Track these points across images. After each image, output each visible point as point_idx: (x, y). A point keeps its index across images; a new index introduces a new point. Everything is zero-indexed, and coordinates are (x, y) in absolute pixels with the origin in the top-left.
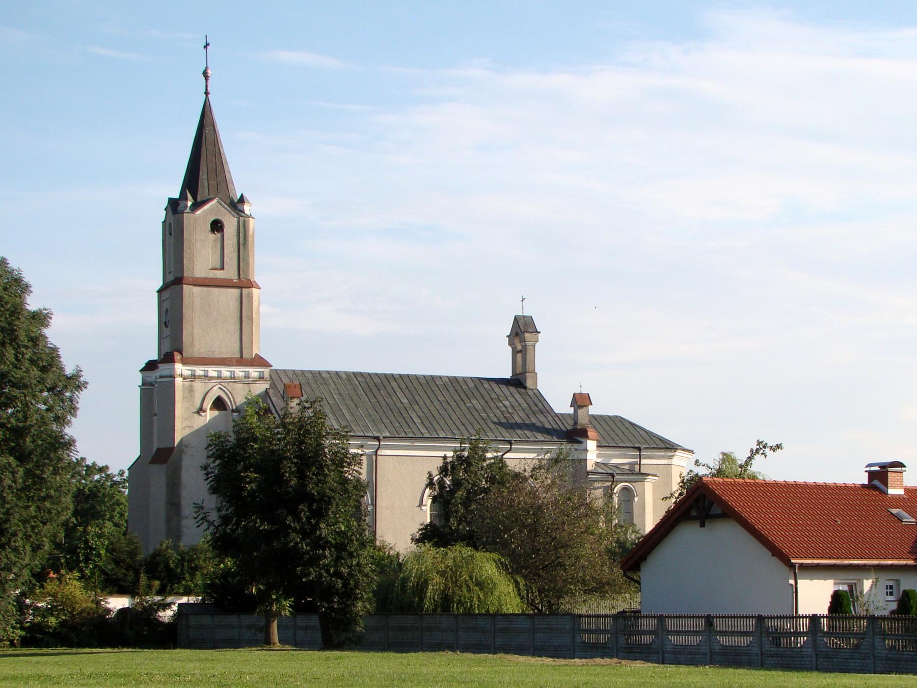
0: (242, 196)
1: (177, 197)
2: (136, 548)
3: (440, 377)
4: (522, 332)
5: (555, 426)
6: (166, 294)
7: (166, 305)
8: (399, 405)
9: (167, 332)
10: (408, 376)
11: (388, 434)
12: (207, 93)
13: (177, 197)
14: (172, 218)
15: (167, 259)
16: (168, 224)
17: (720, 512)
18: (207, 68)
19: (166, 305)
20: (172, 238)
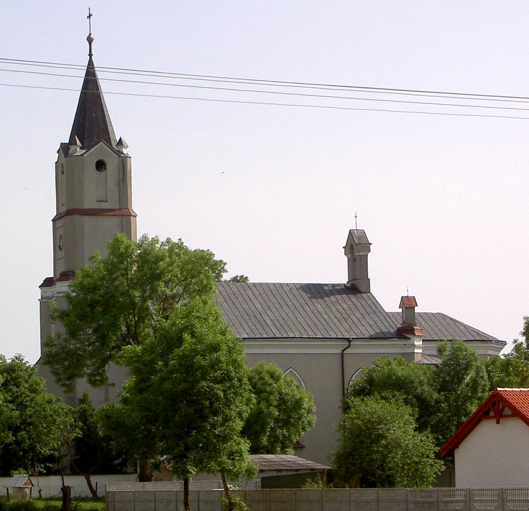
0: (120, 138)
1: (68, 142)
2: (106, 416)
3: (287, 284)
4: (357, 248)
5: (384, 330)
6: (60, 223)
7: (60, 232)
8: (254, 310)
9: (61, 254)
10: (261, 284)
11: (246, 336)
12: (91, 55)
13: (67, 142)
14: (63, 160)
15: (60, 191)
16: (60, 164)
17: (84, 155)
18: (90, 34)
19: (60, 232)
20: (64, 176)
